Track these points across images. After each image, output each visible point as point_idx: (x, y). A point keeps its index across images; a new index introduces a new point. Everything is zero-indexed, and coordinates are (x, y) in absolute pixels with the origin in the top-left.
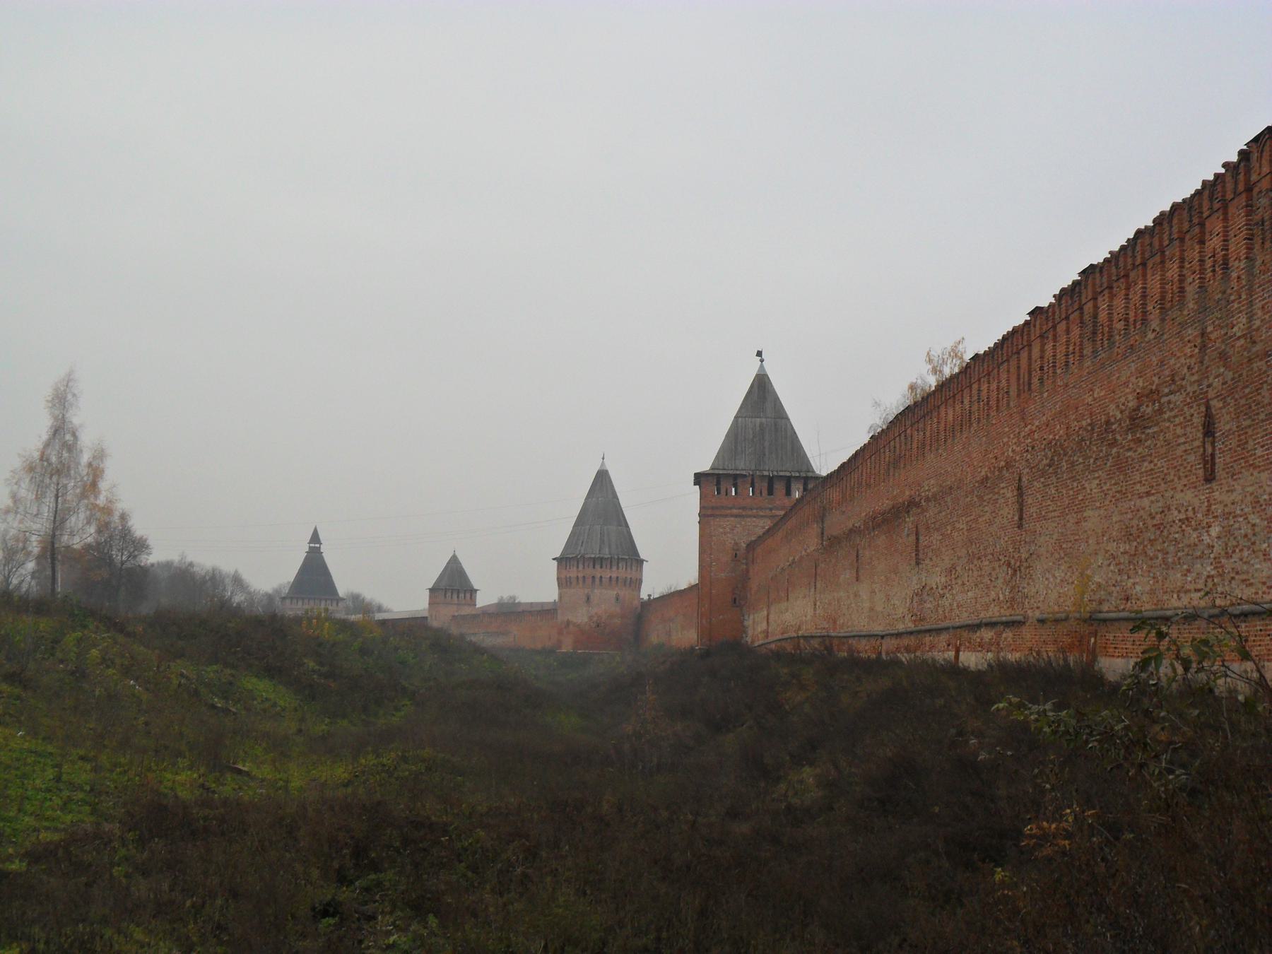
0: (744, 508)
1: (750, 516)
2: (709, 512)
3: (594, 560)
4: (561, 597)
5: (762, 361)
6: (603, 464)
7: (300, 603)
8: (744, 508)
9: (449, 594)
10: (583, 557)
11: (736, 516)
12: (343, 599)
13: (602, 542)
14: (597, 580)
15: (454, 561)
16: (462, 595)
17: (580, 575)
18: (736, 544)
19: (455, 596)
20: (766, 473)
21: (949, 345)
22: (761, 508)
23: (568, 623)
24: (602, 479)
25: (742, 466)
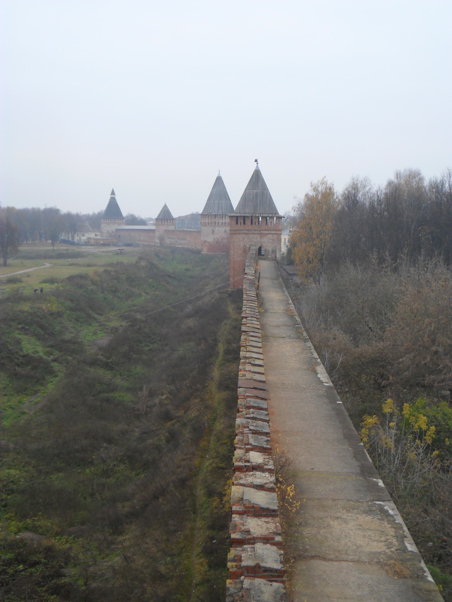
0: (248, 230)
2: (233, 232)
3: (215, 216)
5: (257, 164)
6: (219, 173)
7: (108, 220)
8: (248, 230)
9: (163, 221)
10: (211, 214)
11: (245, 234)
12: (125, 218)
13: (219, 207)
14: (217, 224)
15: (165, 206)
16: (169, 221)
17: (210, 222)
18: (245, 246)
19: (166, 222)
22: (255, 230)
23: (205, 241)
24: (219, 180)
25: (247, 211)
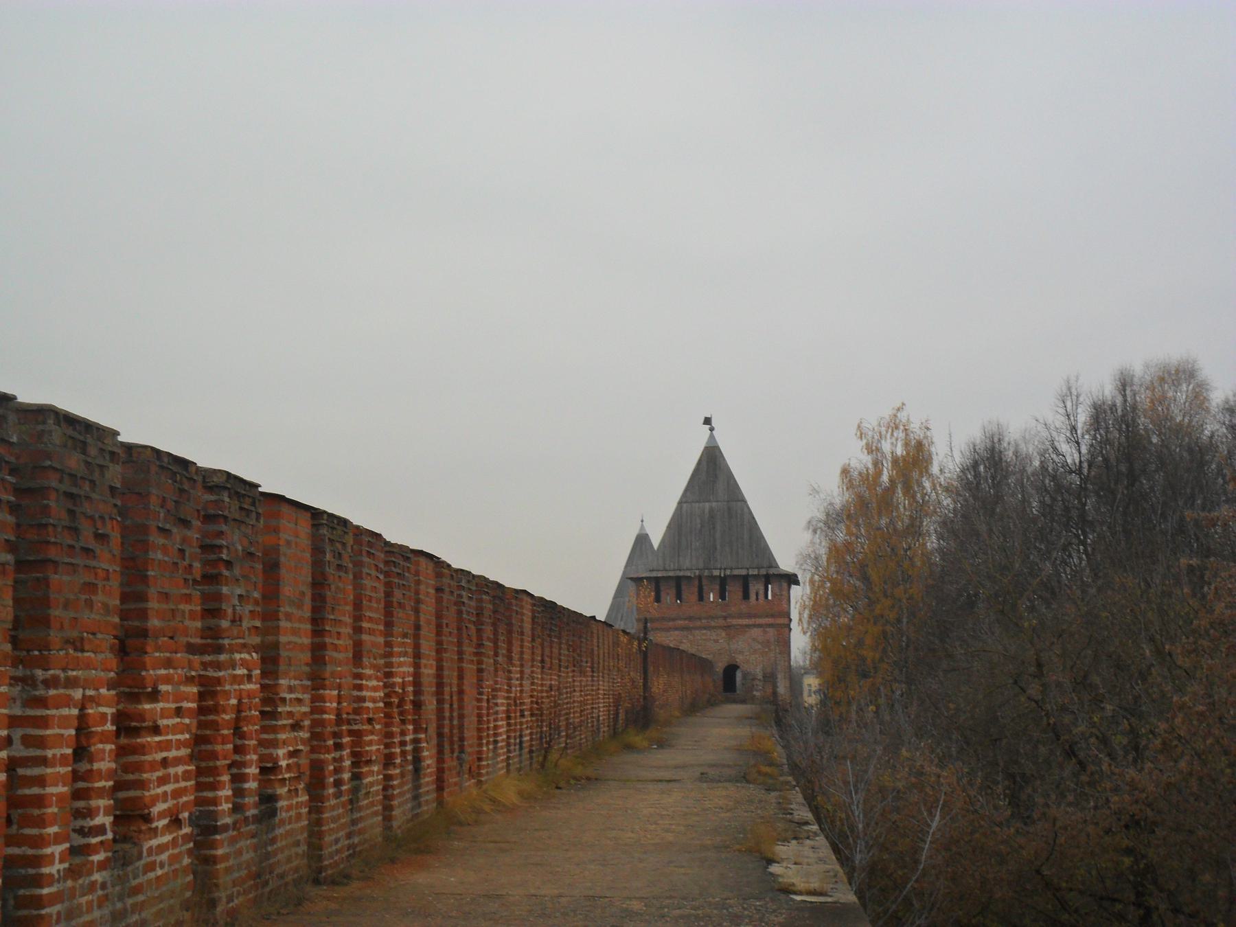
0: (690, 618)
1: (700, 628)
4: (789, 588)
5: (712, 429)
8: (690, 618)
20: (716, 573)
21: (887, 413)
22: (712, 618)
